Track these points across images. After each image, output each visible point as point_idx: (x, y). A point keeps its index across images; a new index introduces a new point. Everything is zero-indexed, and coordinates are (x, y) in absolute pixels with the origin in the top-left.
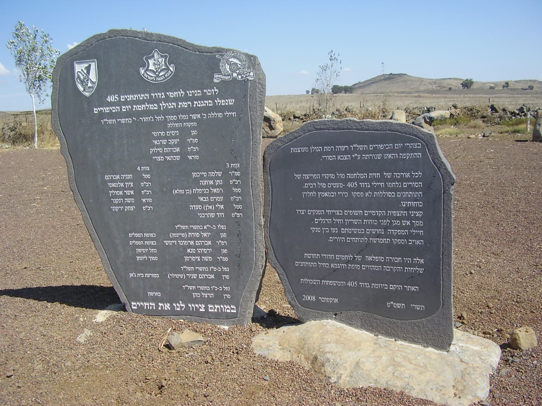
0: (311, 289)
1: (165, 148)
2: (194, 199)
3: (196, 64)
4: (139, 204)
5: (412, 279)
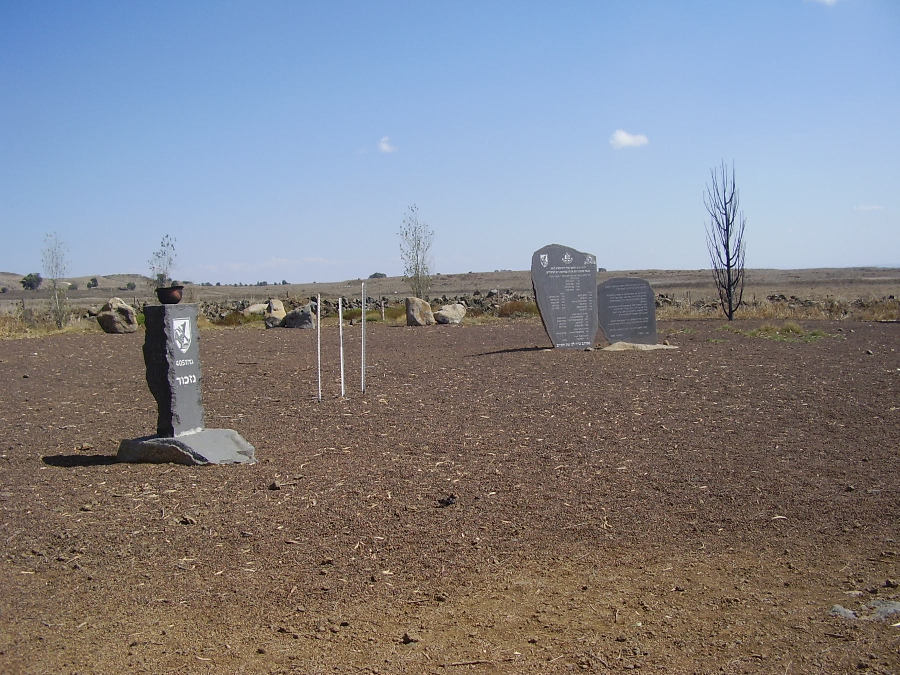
0: (613, 333)
1: (569, 287)
2: (578, 304)
3: (580, 258)
4: (561, 307)
5: (645, 325)
